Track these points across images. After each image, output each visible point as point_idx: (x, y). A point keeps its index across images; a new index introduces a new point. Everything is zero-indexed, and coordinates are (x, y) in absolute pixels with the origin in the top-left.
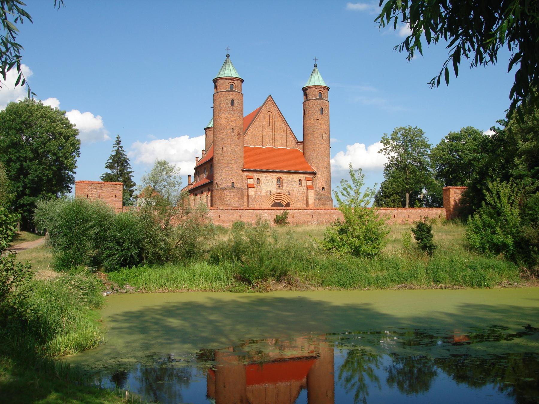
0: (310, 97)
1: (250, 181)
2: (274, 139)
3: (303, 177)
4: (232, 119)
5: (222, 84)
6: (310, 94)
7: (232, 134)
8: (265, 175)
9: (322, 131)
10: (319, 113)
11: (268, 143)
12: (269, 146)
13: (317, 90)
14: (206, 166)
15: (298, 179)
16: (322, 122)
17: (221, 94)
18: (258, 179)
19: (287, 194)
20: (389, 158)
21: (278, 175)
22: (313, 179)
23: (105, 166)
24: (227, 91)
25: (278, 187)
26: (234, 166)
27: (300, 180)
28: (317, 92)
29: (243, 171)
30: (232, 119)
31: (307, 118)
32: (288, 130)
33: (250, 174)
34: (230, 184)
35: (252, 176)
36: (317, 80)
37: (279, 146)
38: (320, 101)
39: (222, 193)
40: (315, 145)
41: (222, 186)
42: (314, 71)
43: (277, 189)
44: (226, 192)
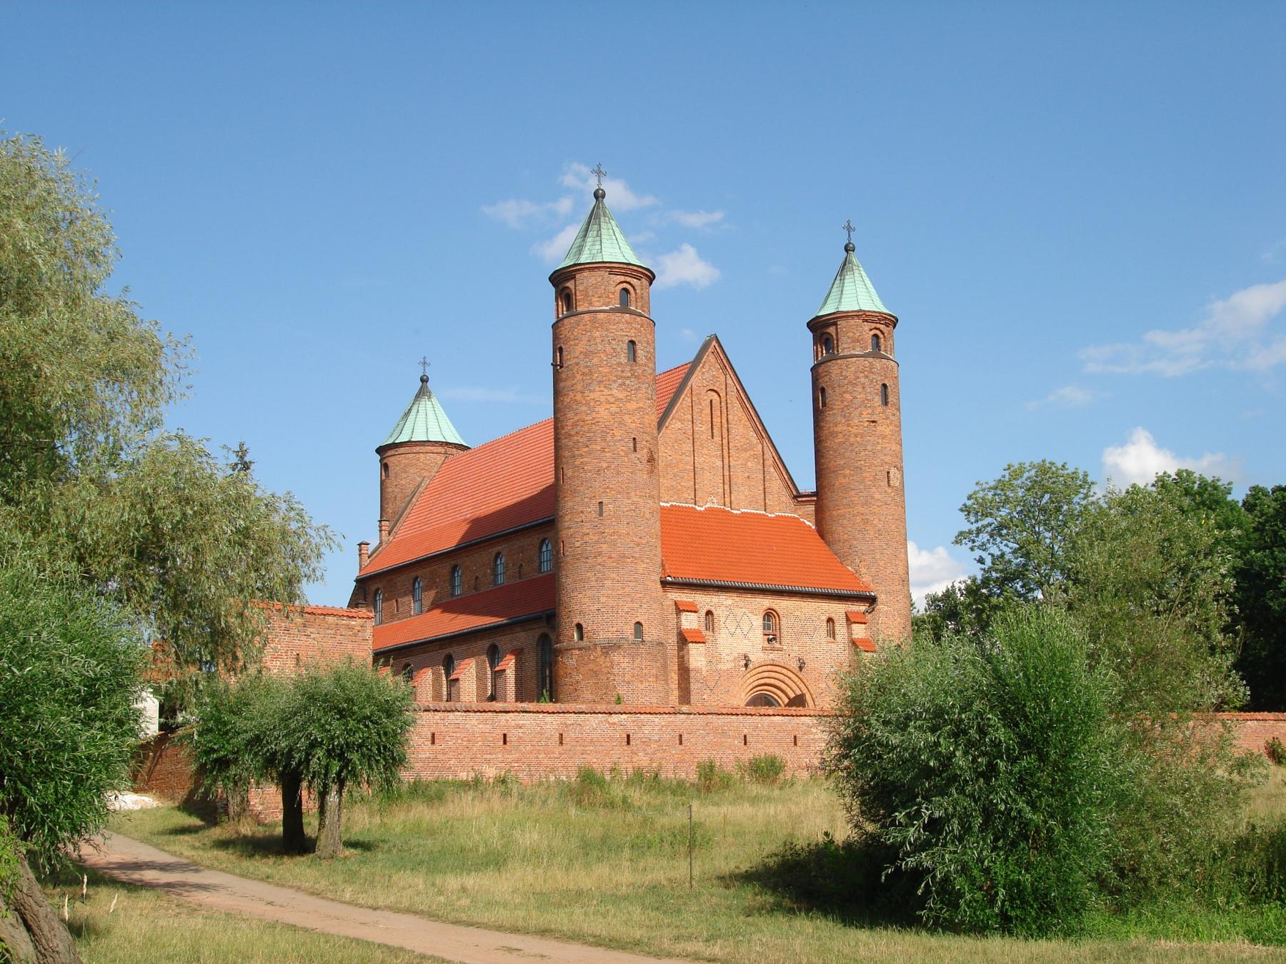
0: (845, 347)
1: (690, 622)
2: (728, 481)
3: (838, 609)
4: (632, 406)
5: (595, 286)
6: (843, 339)
7: (633, 456)
8: (729, 602)
9: (888, 459)
10: (878, 400)
11: (711, 494)
12: (714, 503)
13: (867, 326)
14: (419, 573)
15: (824, 618)
16: (887, 431)
17: (593, 321)
18: (709, 613)
19: (794, 665)
20: (981, 561)
21: (766, 602)
22: (869, 617)
23: (960, 506)
24: (612, 311)
25: (766, 644)
26: (641, 567)
27: (830, 620)
28: (866, 331)
29: (664, 584)
30: (632, 406)
31: (834, 418)
32: (769, 454)
33: (684, 597)
34: (629, 631)
35: (692, 604)
36: (859, 295)
37: (743, 506)
38: (878, 364)
39: (601, 660)
40: (866, 504)
41: (603, 636)
42: (845, 266)
43: (764, 649)
44: (616, 657)
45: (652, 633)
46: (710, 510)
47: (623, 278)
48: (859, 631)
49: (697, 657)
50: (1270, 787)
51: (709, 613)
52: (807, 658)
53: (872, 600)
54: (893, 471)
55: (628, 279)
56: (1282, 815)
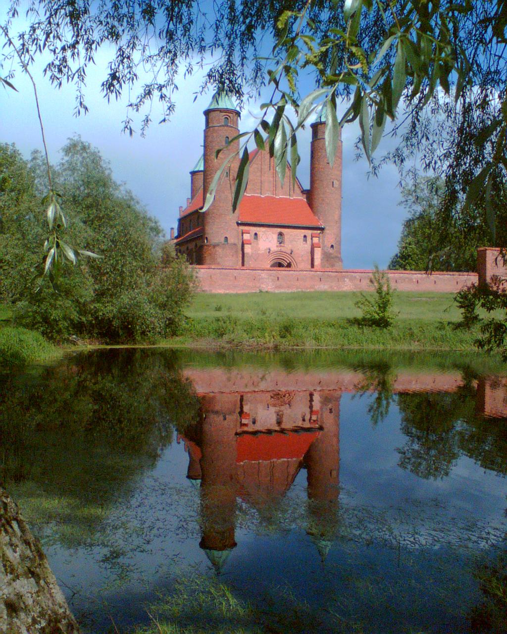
3: (308, 233)
21: (279, 230)
25: (278, 245)
29: (238, 224)
34: (223, 240)
35: (249, 231)
45: (231, 241)
46: (267, 197)
47: (225, 114)
48: (316, 240)
49: (248, 249)
50: (502, 316)
51: (256, 234)
52: (294, 250)
53: (322, 229)
54: (335, 182)
55: (227, 114)
56: (503, 290)
